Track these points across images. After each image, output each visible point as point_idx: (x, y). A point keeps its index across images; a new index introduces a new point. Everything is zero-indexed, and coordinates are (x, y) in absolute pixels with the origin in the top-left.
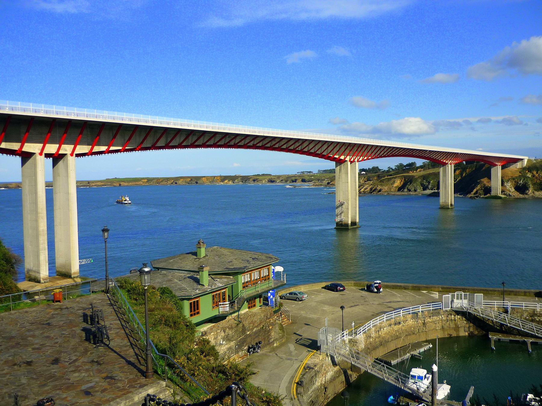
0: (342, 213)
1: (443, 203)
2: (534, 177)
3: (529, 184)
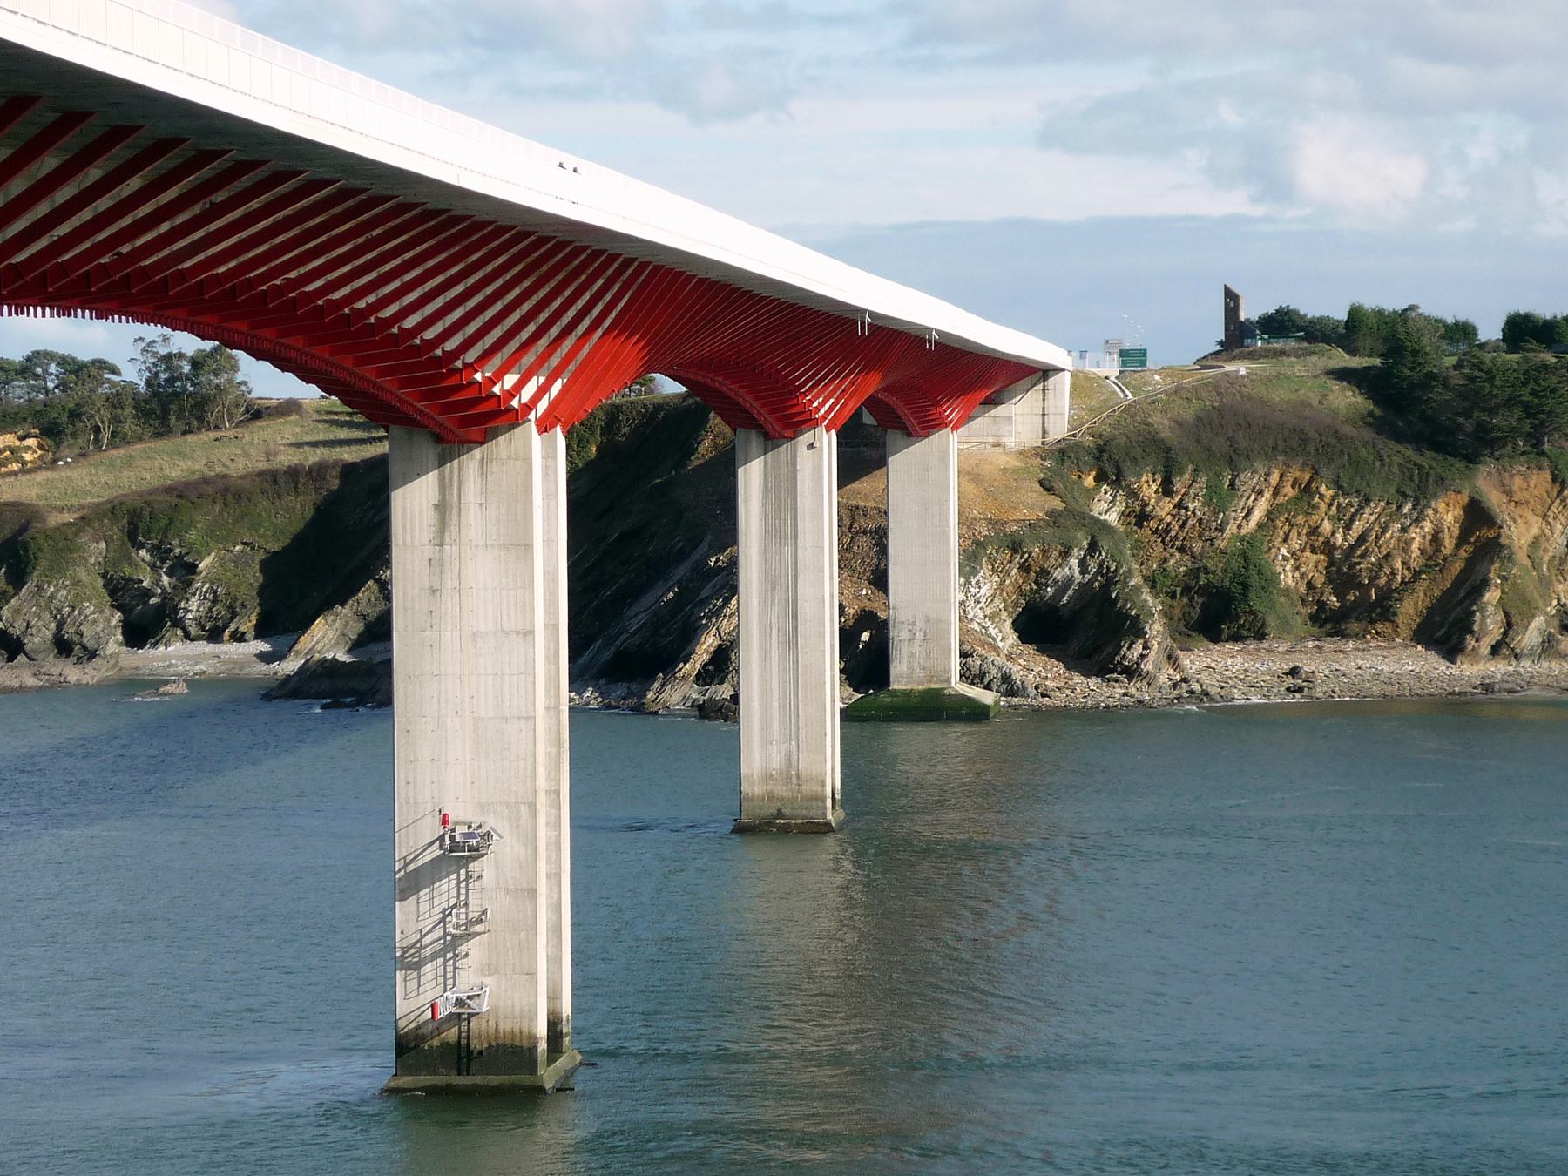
0: (468, 936)
1: (768, 777)
2: (1140, 526)
3: (1136, 589)
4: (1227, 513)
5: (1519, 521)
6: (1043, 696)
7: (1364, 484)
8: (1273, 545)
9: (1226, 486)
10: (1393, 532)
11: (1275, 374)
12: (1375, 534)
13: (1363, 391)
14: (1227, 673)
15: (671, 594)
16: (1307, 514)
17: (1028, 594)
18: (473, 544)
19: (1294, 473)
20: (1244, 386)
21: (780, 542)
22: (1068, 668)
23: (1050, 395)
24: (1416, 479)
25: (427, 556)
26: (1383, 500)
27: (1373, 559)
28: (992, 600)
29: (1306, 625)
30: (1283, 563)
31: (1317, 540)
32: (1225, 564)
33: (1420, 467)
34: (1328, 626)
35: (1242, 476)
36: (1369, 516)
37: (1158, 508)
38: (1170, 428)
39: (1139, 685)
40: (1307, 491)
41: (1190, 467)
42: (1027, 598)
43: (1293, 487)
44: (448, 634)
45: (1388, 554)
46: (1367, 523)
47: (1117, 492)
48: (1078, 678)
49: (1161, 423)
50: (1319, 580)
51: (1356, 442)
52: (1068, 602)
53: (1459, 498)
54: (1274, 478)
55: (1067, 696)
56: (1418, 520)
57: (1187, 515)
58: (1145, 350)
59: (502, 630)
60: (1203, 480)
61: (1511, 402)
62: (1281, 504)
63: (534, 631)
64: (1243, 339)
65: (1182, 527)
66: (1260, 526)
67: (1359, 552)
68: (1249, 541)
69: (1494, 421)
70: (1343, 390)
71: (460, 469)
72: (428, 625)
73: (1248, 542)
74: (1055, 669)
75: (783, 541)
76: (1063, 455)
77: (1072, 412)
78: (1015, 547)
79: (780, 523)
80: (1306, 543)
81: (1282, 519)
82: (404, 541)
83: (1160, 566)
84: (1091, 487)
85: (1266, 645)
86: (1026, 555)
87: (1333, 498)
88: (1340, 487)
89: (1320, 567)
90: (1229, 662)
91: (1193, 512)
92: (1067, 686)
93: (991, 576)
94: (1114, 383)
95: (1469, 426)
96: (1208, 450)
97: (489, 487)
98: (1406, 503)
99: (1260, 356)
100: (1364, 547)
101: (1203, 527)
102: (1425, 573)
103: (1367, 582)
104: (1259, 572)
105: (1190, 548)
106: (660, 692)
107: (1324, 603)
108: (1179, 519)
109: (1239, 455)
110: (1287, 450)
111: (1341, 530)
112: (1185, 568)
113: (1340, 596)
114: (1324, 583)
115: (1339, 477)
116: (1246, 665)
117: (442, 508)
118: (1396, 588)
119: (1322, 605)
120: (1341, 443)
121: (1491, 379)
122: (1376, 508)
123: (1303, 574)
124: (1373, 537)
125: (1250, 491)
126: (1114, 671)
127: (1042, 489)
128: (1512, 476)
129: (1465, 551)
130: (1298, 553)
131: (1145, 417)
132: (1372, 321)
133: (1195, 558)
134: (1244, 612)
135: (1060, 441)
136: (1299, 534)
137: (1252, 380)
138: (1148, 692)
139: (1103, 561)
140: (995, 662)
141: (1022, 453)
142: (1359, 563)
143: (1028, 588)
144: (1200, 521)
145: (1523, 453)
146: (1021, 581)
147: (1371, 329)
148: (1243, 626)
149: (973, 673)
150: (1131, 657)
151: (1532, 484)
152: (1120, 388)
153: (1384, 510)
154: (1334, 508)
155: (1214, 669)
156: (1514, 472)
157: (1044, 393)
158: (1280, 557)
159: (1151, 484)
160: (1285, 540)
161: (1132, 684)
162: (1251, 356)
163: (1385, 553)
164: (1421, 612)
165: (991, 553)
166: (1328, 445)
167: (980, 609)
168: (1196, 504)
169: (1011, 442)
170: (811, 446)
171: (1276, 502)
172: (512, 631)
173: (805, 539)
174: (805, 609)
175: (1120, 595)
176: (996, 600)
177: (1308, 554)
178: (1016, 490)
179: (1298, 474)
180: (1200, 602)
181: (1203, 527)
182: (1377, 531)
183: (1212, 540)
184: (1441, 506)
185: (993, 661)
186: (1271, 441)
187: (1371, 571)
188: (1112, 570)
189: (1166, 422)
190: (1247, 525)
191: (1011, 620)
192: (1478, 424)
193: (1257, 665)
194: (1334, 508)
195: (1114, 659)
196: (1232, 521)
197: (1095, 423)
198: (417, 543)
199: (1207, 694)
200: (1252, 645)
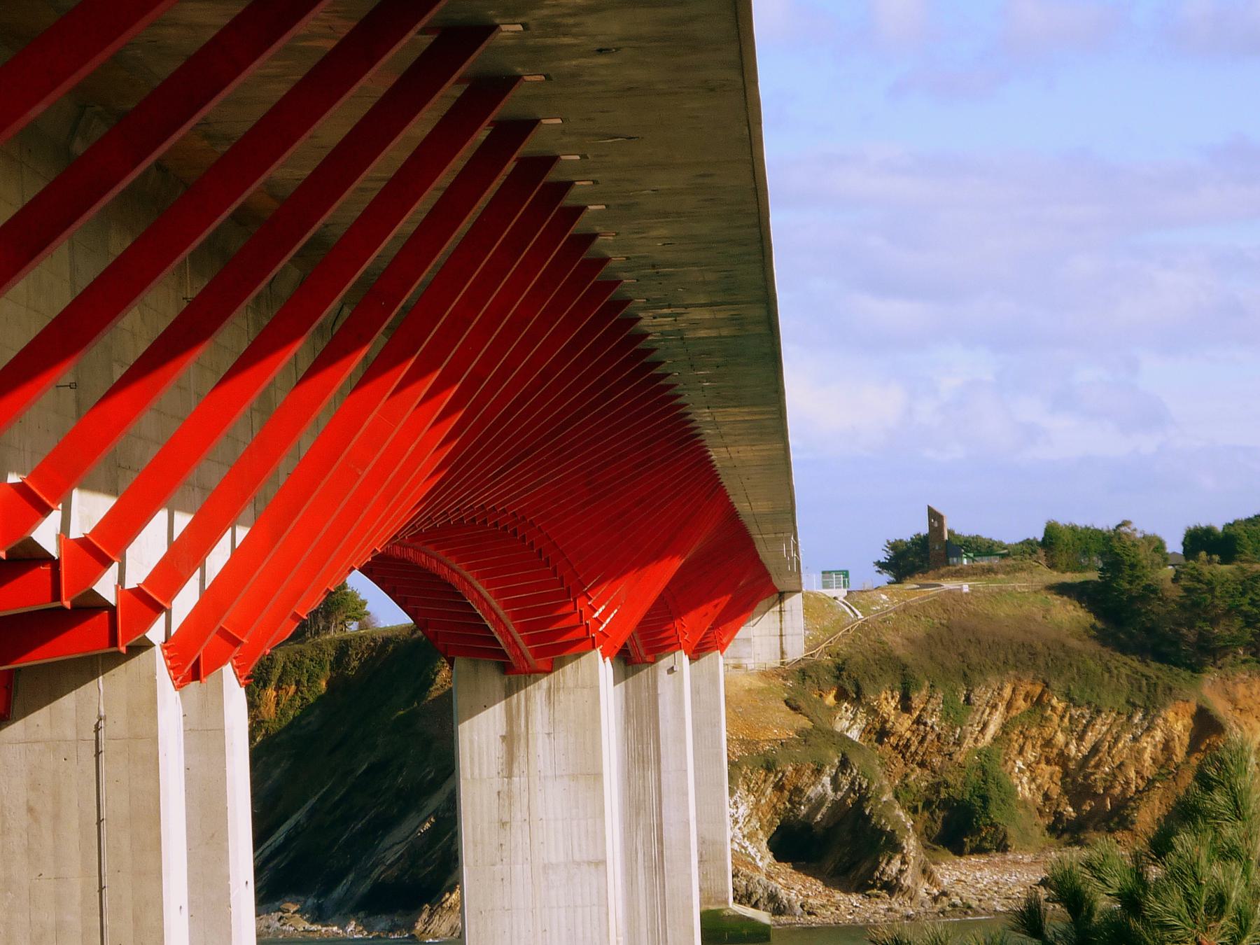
4: (964, 727)
5: (1245, 727)
6: (809, 913)
7: (1095, 696)
8: (1010, 758)
9: (962, 702)
10: (1125, 742)
11: (998, 590)
12: (1107, 744)
13: (1084, 605)
14: (978, 886)
15: (428, 825)
16: (1041, 726)
17: (782, 812)
18: (542, 774)
19: (1026, 687)
20: (970, 603)
21: (643, 766)
22: (826, 885)
23: (787, 616)
24: (1145, 689)
25: (496, 787)
26: (1113, 711)
27: (1107, 769)
28: (749, 820)
29: (1044, 835)
30: (1019, 775)
31: (1051, 752)
32: (964, 777)
33: (1147, 678)
34: (1066, 837)
35: (977, 691)
36: (1101, 727)
37: (897, 725)
38: (903, 645)
39: (901, 899)
40: (1039, 703)
41: (927, 683)
42: (782, 817)
43: (1025, 700)
44: (519, 867)
45: (1122, 764)
46: (1099, 734)
47: (858, 709)
48: (839, 896)
49: (895, 641)
50: (1055, 791)
51: (1084, 655)
52: (822, 820)
53: (1187, 707)
54: (1007, 692)
55: (832, 913)
56: (1148, 729)
57: (926, 730)
58: (847, 571)
59: (574, 861)
60: (940, 695)
61: (1230, 612)
62: (1015, 718)
63: (606, 862)
64: (948, 558)
65: (921, 742)
66: (995, 739)
67: (1093, 763)
68: (986, 754)
69: (1216, 631)
70: (1064, 604)
71: (527, 699)
72: (498, 860)
73: (986, 756)
74: (814, 887)
75: (646, 766)
76: (804, 675)
77: (807, 632)
78: (769, 767)
79: (643, 747)
80: (1041, 755)
81: (1016, 732)
82: (472, 774)
83: (902, 781)
84: (832, 705)
85: (1010, 856)
86: (780, 775)
87: (1065, 710)
88: (1071, 700)
89: (1055, 779)
90: (978, 874)
91: (932, 727)
92: (830, 903)
93: (747, 796)
94: (843, 603)
95: (1191, 636)
96: (942, 665)
97: (556, 715)
98: (1136, 713)
99: (968, 574)
100: (1097, 758)
101: (942, 741)
102: (1158, 781)
103: (1102, 792)
104: (999, 785)
105: (930, 763)
106: (428, 923)
107: (1061, 814)
108: (918, 735)
109: (972, 670)
110: (1018, 664)
111: (1074, 741)
112: (926, 783)
113: (1077, 807)
114: (1060, 794)
115: (1069, 689)
116: (995, 877)
117: (510, 740)
118: (1131, 798)
119: (1058, 816)
120: (1069, 657)
121: (1212, 590)
122: (1107, 719)
123: (1039, 786)
124: (1107, 747)
125: (984, 705)
126: (873, 887)
127: (788, 709)
128: (1235, 684)
129: (1196, 758)
130: (1034, 765)
131: (878, 635)
132: (1067, 537)
133: (935, 772)
134: (986, 825)
135: (799, 661)
136: (1034, 746)
137: (976, 597)
138: (911, 907)
139: (855, 778)
140: (761, 882)
141: (764, 674)
142: (1093, 774)
143: (782, 807)
144: (939, 736)
145: (1244, 662)
146: (775, 800)
147: (1067, 545)
148: (985, 839)
149: (740, 893)
150: (890, 872)
151: (1255, 692)
152: (850, 608)
153: (1115, 721)
154: (1066, 720)
155: (965, 882)
156: (1237, 680)
157: (781, 615)
158: (1017, 770)
159: (890, 700)
160: (1021, 752)
161: (893, 899)
162: (958, 574)
163: (1118, 763)
164: (1158, 819)
165: (746, 773)
166: (1057, 658)
167: (739, 829)
168: (934, 720)
169: (751, 663)
170: (671, 670)
171: (1010, 715)
172: (584, 862)
173: (668, 763)
174: (671, 834)
175: (874, 812)
176: (753, 820)
177: (1043, 765)
178: (765, 709)
179: (1029, 688)
180: (941, 816)
181: (942, 741)
182: (1109, 742)
183: (950, 755)
184: (1171, 716)
185: (758, 881)
186: (1001, 656)
187: (1105, 781)
188: (864, 786)
189: (898, 639)
190: (983, 738)
191: (766, 839)
192: (1200, 634)
193: (1005, 877)
194: (1066, 720)
195: (873, 875)
196: (969, 735)
197: (831, 642)
198: (485, 775)
199: (970, 907)
200: (997, 858)
